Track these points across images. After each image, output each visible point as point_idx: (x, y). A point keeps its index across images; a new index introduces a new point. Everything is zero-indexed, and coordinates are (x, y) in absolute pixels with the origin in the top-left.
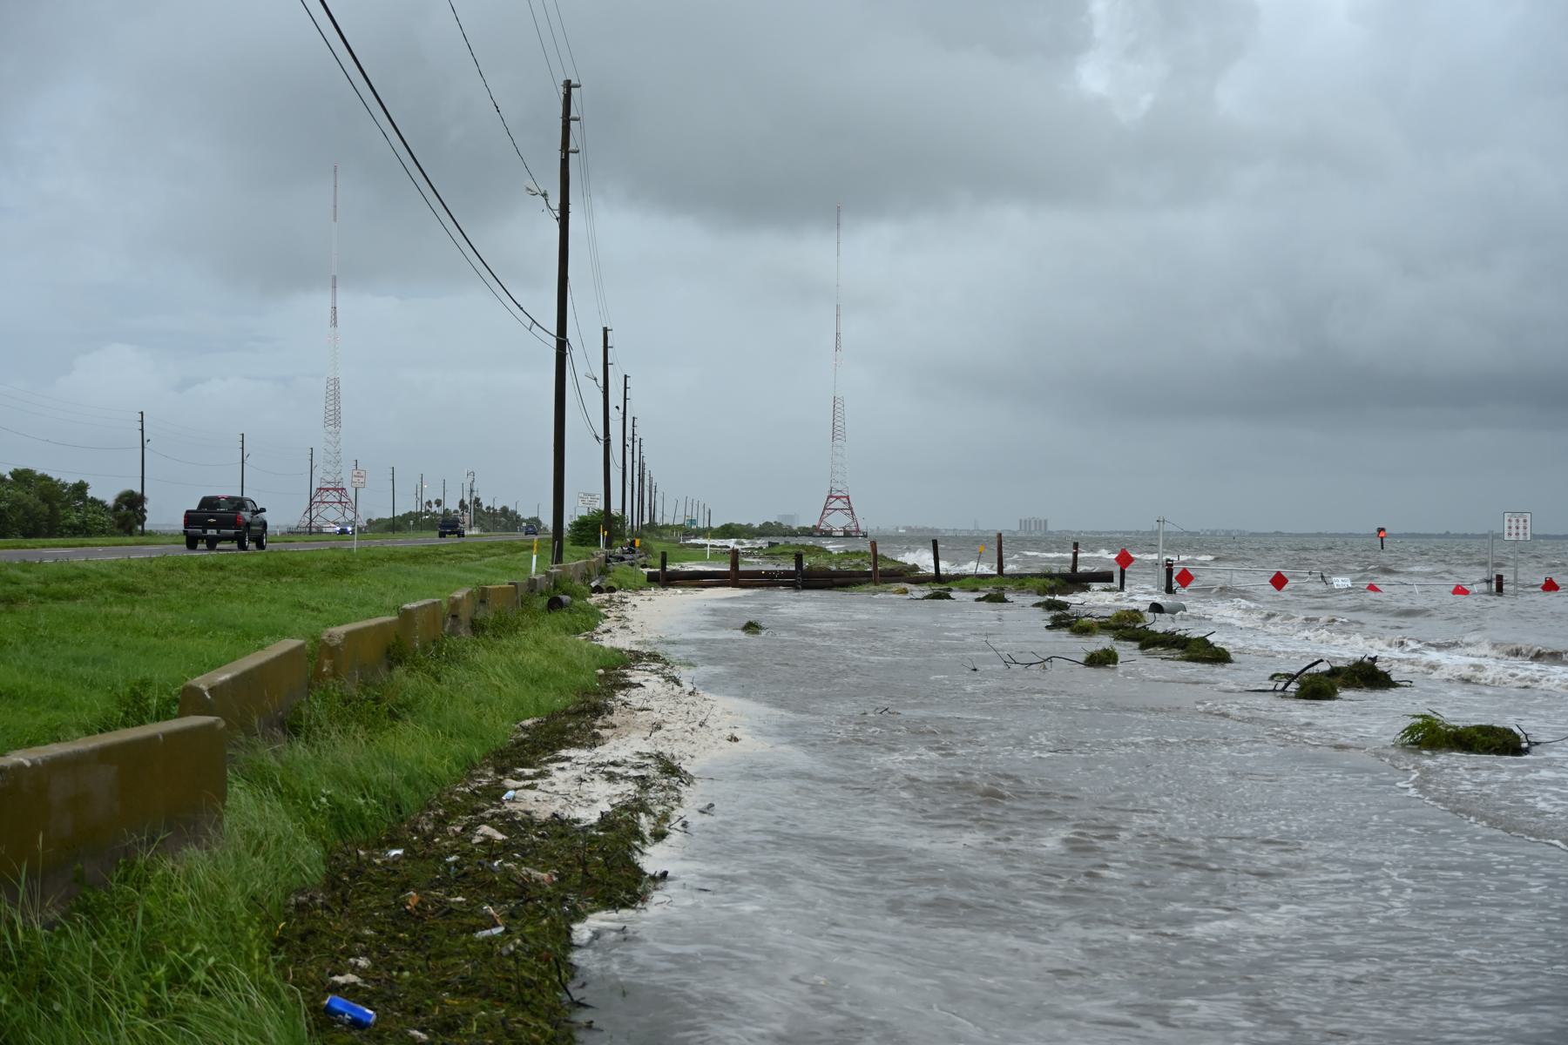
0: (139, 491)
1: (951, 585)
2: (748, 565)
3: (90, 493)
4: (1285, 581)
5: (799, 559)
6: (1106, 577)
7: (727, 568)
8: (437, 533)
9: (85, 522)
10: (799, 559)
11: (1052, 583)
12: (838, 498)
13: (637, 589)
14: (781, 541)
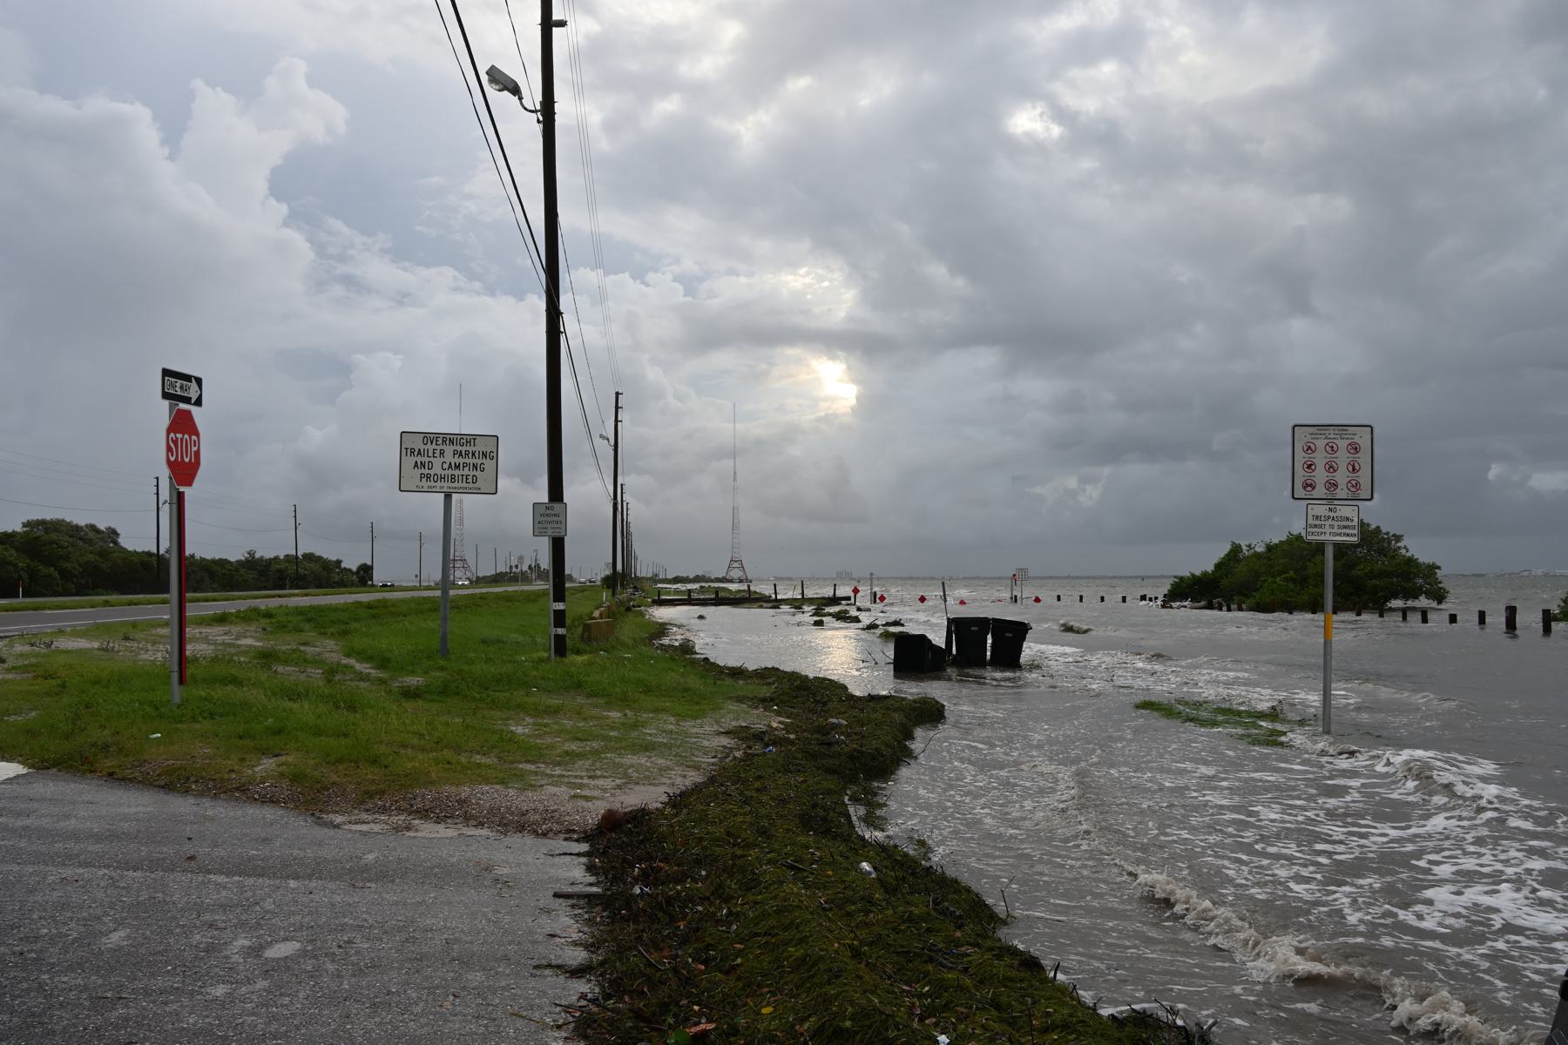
0: (369, 563)
1: (782, 603)
2: (695, 596)
3: (343, 565)
4: (923, 602)
5: (717, 593)
6: (848, 598)
7: (713, 596)
8: (379, 577)
9: (343, 580)
10: (717, 593)
11: (824, 601)
12: (736, 561)
13: (650, 606)
14: (706, 585)
